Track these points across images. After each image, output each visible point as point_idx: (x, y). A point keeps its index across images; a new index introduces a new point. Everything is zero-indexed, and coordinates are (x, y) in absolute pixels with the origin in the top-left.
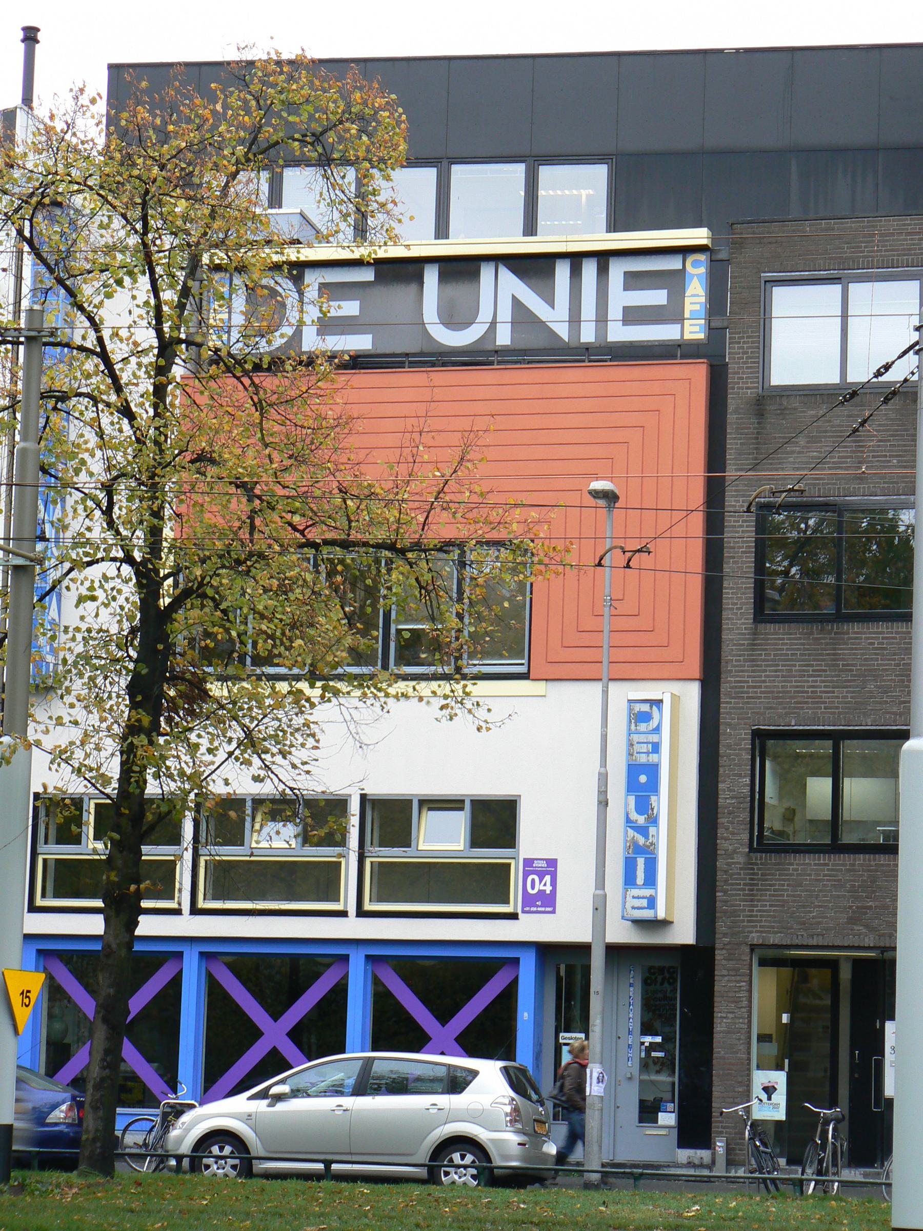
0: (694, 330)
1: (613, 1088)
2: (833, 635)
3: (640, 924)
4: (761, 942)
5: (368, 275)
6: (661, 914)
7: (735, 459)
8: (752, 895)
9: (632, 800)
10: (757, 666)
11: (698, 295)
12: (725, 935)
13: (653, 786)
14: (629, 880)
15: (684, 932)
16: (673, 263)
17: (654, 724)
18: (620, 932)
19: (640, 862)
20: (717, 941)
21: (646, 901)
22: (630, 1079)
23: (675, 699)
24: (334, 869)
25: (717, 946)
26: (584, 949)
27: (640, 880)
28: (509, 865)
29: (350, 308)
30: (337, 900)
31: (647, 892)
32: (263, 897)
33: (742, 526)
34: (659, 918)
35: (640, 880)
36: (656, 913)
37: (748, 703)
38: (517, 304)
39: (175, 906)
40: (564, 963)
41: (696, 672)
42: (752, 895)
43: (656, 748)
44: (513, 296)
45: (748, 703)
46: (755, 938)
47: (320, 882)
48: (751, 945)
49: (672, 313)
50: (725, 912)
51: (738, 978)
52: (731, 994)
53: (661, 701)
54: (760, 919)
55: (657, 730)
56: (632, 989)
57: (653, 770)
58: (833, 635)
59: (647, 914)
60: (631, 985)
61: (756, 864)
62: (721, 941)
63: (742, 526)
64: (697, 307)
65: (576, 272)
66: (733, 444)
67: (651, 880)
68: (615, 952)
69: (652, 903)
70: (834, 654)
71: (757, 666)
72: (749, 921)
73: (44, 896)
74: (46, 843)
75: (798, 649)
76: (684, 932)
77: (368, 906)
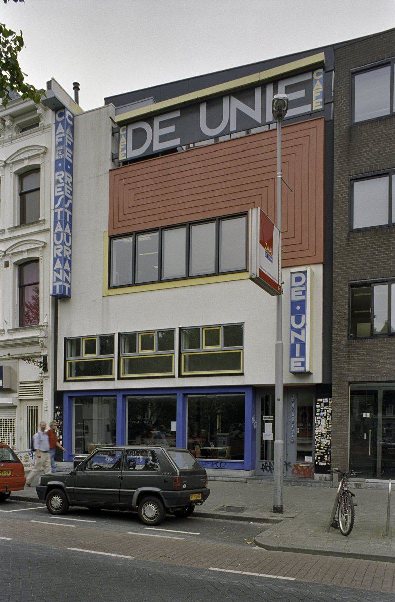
0: (317, 105)
1: (285, 446)
2: (388, 235)
3: (296, 374)
4: (354, 380)
5: (178, 114)
6: (308, 369)
7: (337, 160)
8: (350, 359)
9: (293, 318)
10: (350, 253)
11: (319, 89)
12: (337, 378)
13: (303, 311)
14: (293, 354)
15: (317, 378)
16: (307, 77)
17: (302, 282)
18: (289, 380)
19: (297, 348)
20: (333, 381)
21: (300, 363)
22: (293, 442)
23: (313, 273)
24: (169, 360)
25: (333, 383)
26: (271, 389)
27: (298, 354)
28: (240, 353)
29: (171, 129)
30: (239, 368)
31: (302, 359)
32: (212, 369)
33: (342, 190)
34: (307, 371)
35: (298, 354)
36: (305, 368)
37: (346, 271)
38: (238, 111)
39: (173, 374)
40: (264, 394)
41: (320, 257)
42: (350, 359)
43: (304, 293)
44: (254, 109)
45: (346, 271)
46: (351, 379)
47: (164, 365)
48: (349, 382)
49: (308, 100)
50: (337, 368)
51: (343, 397)
52: (339, 405)
53: (306, 271)
54: (354, 371)
55: (305, 284)
56: (293, 404)
57: (303, 304)
58: (388, 235)
59: (302, 369)
60: (293, 403)
61: (351, 345)
62: (335, 381)
63: (342, 190)
64: (319, 94)
65: (264, 93)
66: (337, 152)
67: (303, 354)
68: (288, 389)
69: (303, 364)
70: (388, 244)
71: (350, 253)
72: (348, 371)
73: (185, 371)
74: (71, 356)
75: (371, 243)
76: (317, 378)
77: (183, 373)
